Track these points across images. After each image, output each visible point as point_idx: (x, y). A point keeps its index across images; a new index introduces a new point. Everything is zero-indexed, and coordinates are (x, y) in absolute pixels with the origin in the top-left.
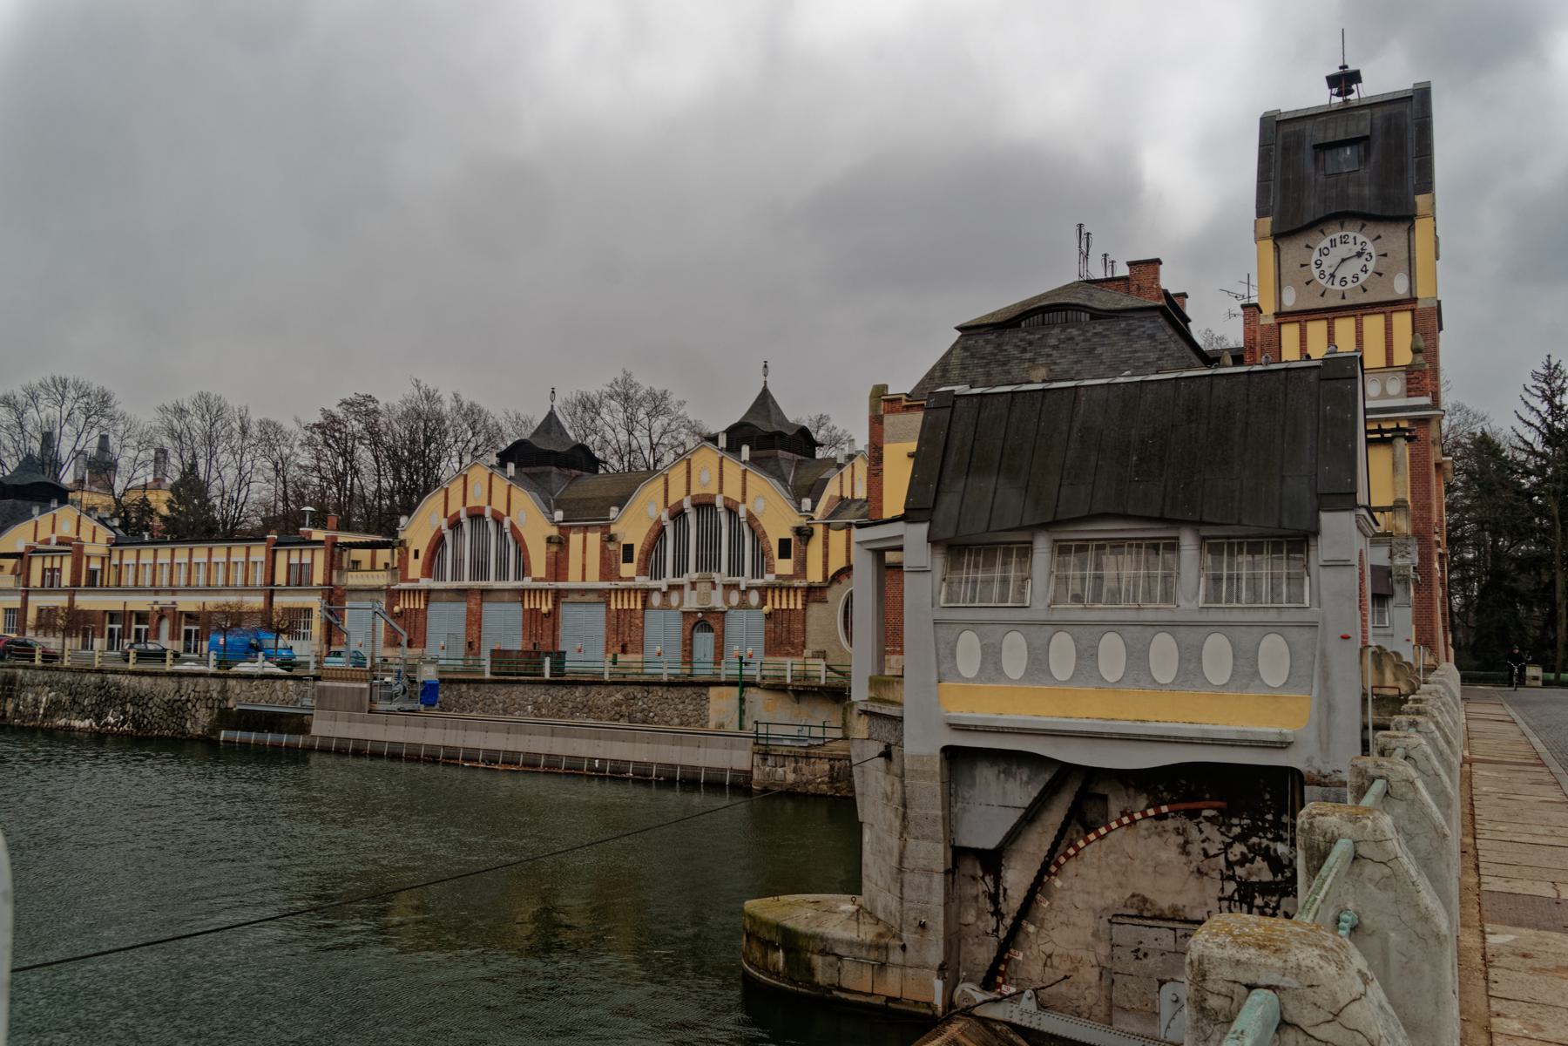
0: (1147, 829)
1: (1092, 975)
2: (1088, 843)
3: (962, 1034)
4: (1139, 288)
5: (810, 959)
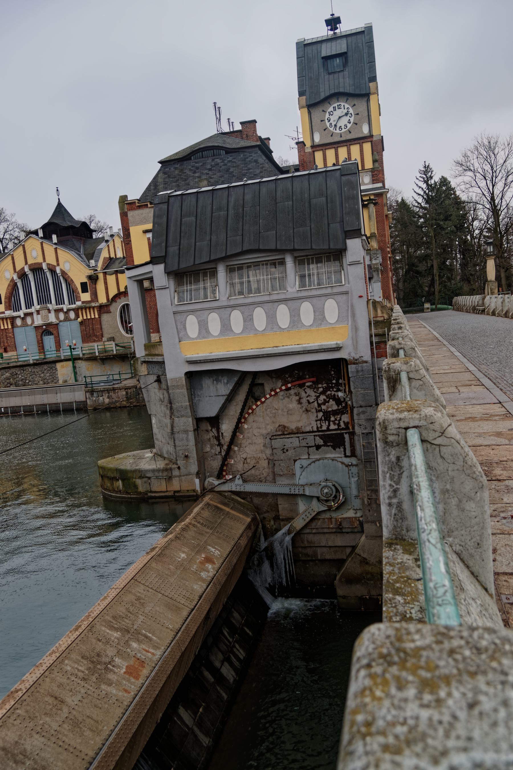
0: (282, 396)
1: (265, 464)
2: (257, 406)
3: (211, 500)
4: (247, 136)
5: (135, 482)
